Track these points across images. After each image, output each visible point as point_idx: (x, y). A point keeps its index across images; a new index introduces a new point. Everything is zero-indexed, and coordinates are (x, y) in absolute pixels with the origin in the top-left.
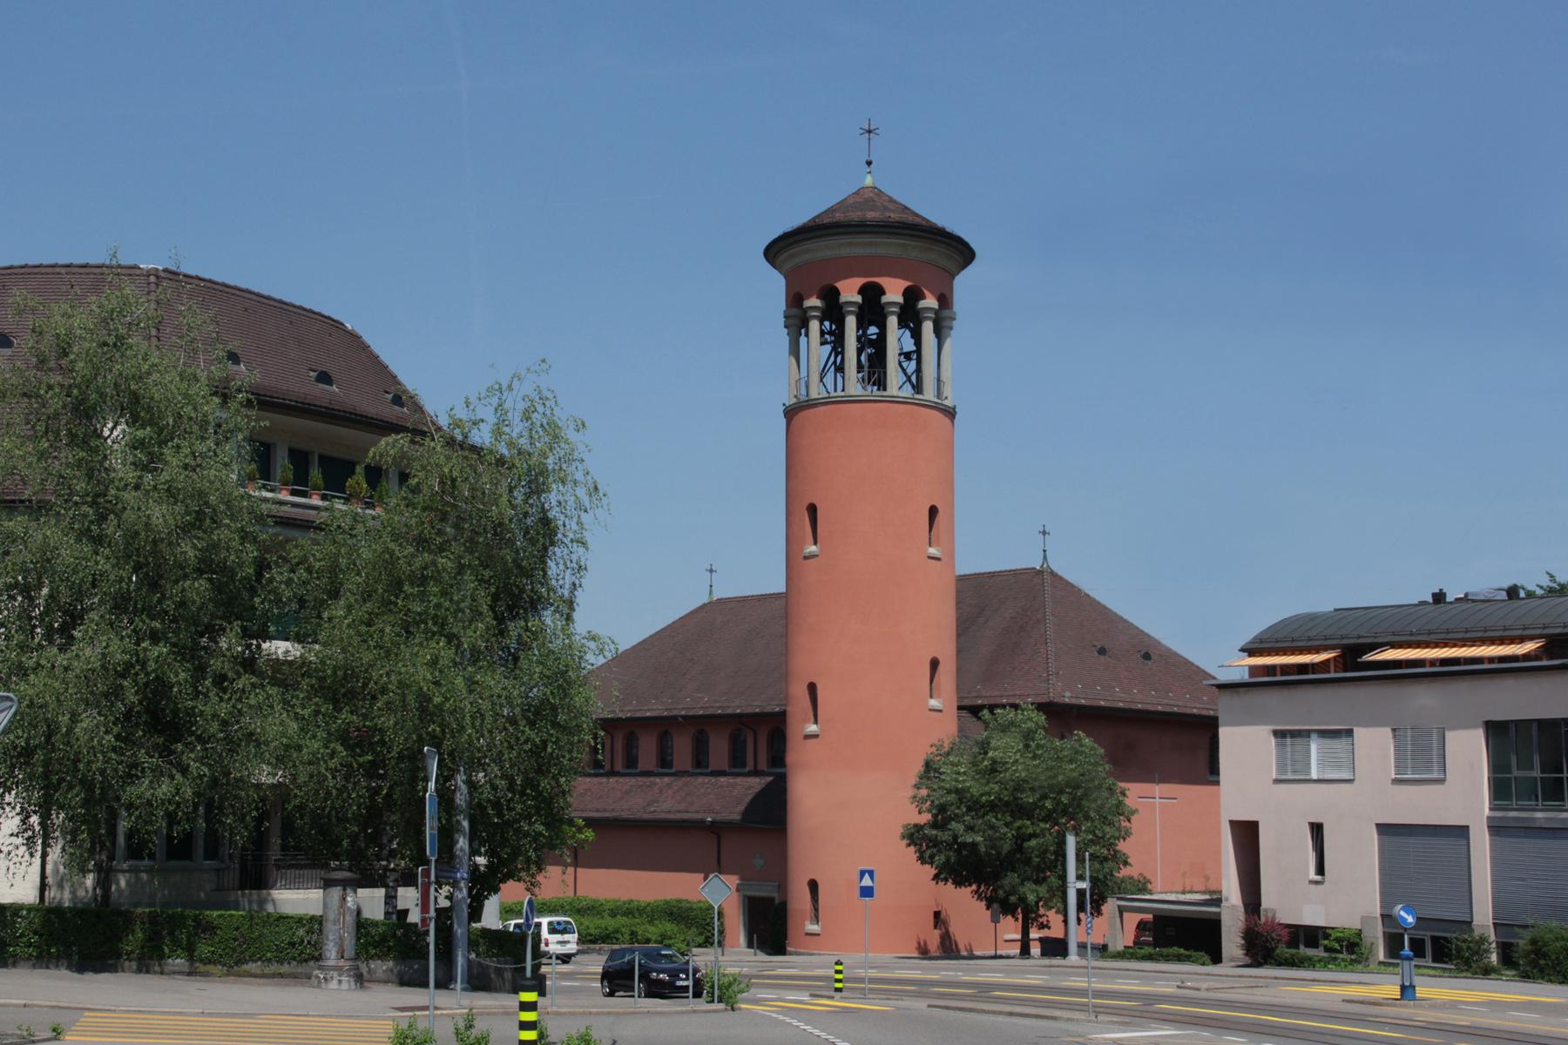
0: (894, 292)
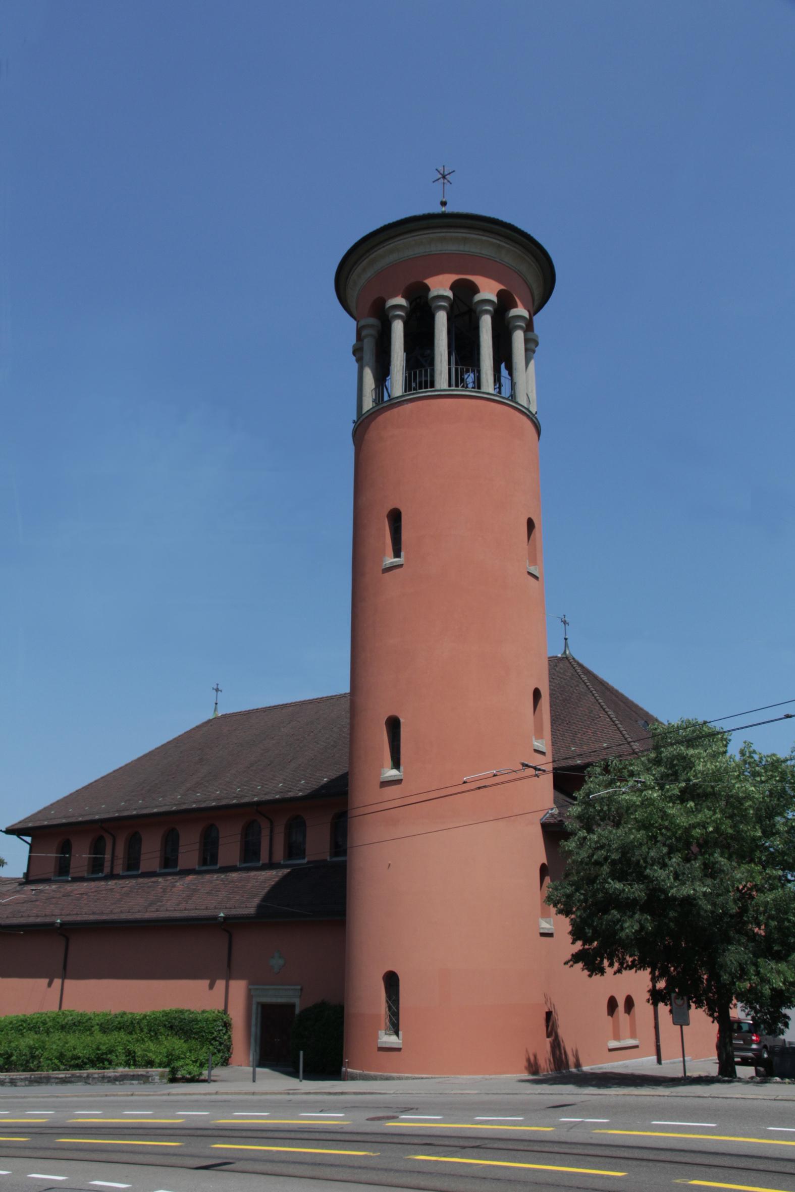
0: (488, 290)
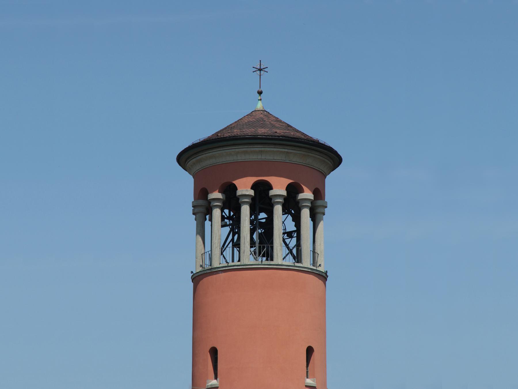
0: (279, 187)
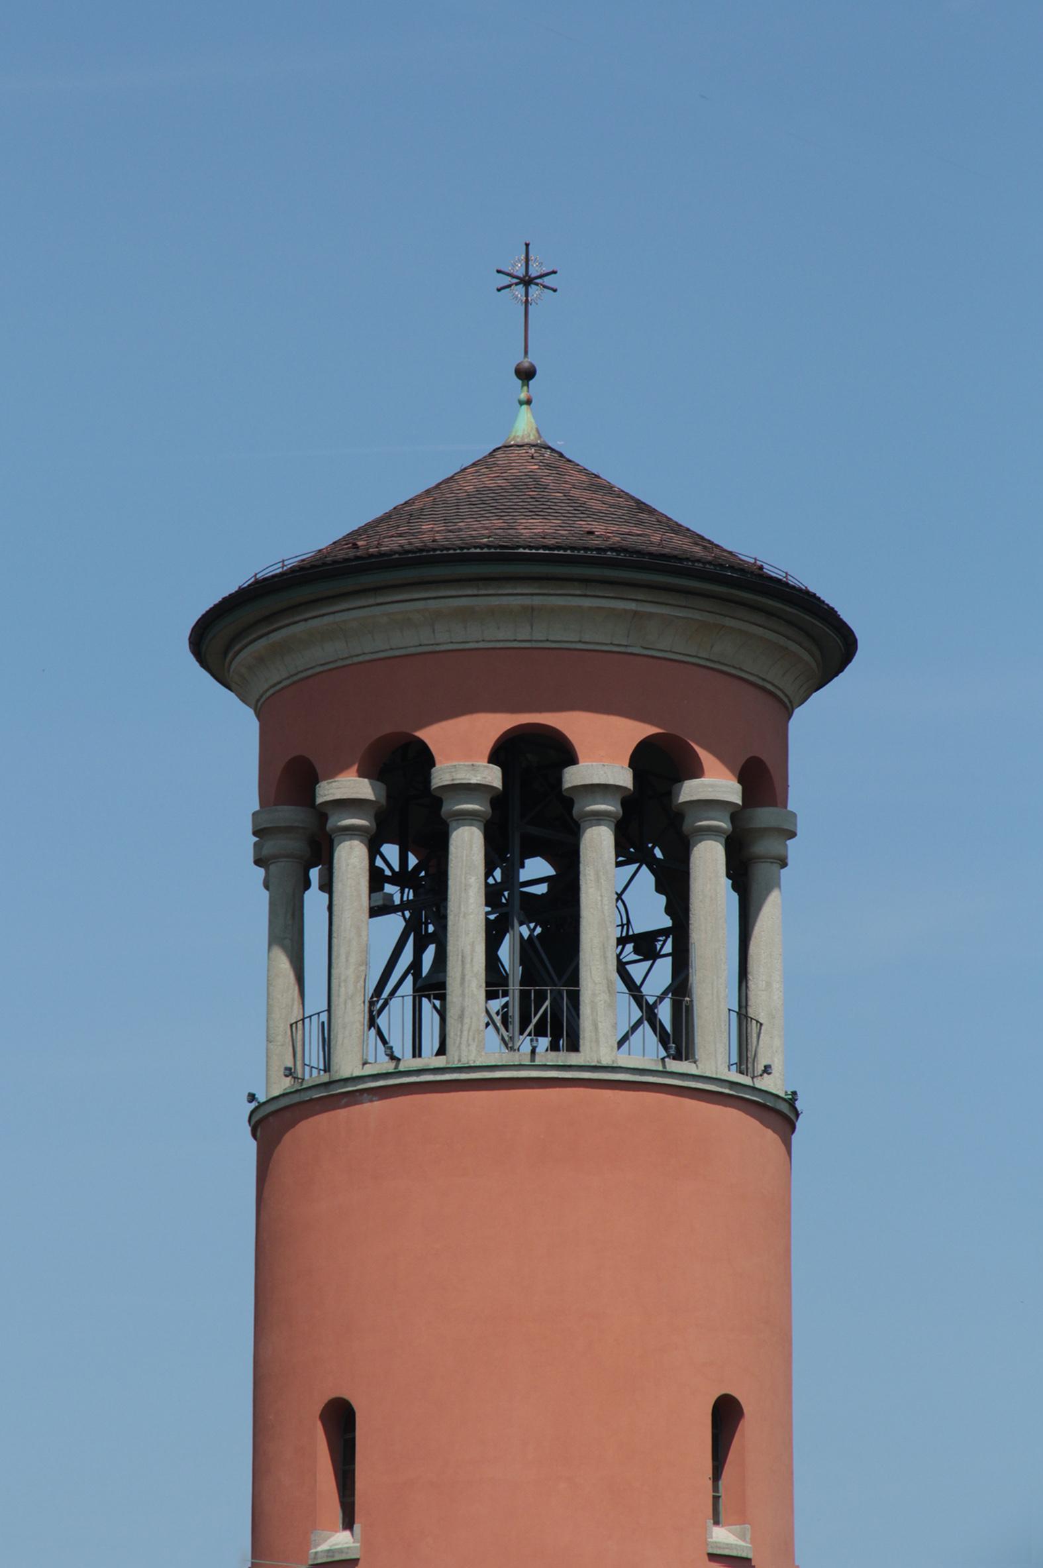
0: (602, 756)
